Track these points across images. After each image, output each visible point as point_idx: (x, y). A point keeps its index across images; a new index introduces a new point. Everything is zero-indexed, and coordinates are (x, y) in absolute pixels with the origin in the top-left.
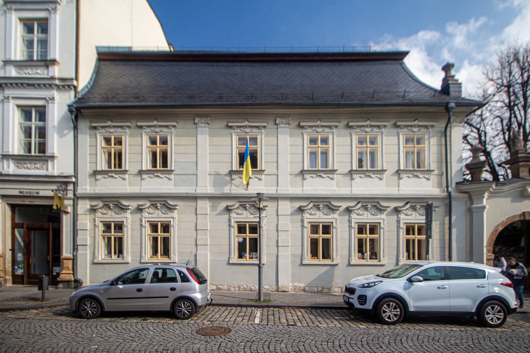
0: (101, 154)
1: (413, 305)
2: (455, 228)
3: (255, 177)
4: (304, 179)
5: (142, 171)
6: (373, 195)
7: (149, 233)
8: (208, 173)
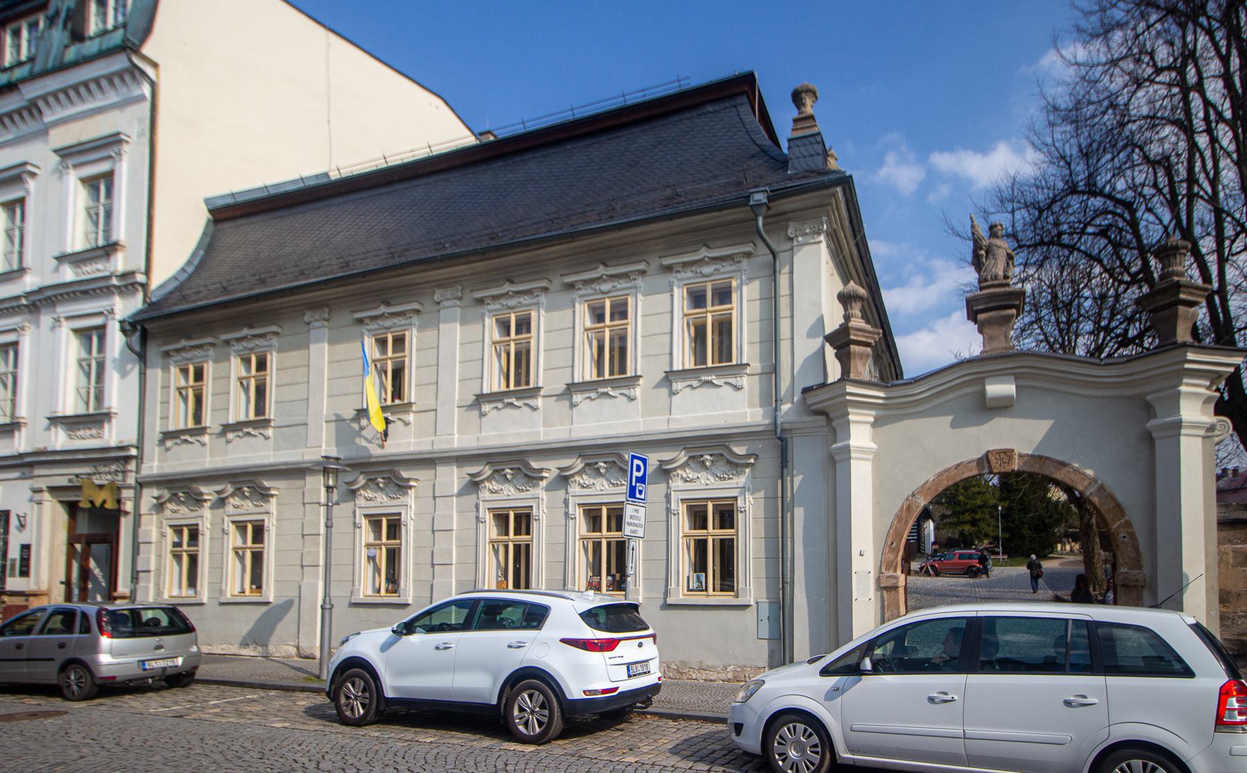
0: (583, 344)
1: (392, 685)
2: (800, 506)
3: (621, 394)
4: (672, 393)
5: (671, 372)
6: (491, 448)
7: (687, 530)
8: (324, 419)
